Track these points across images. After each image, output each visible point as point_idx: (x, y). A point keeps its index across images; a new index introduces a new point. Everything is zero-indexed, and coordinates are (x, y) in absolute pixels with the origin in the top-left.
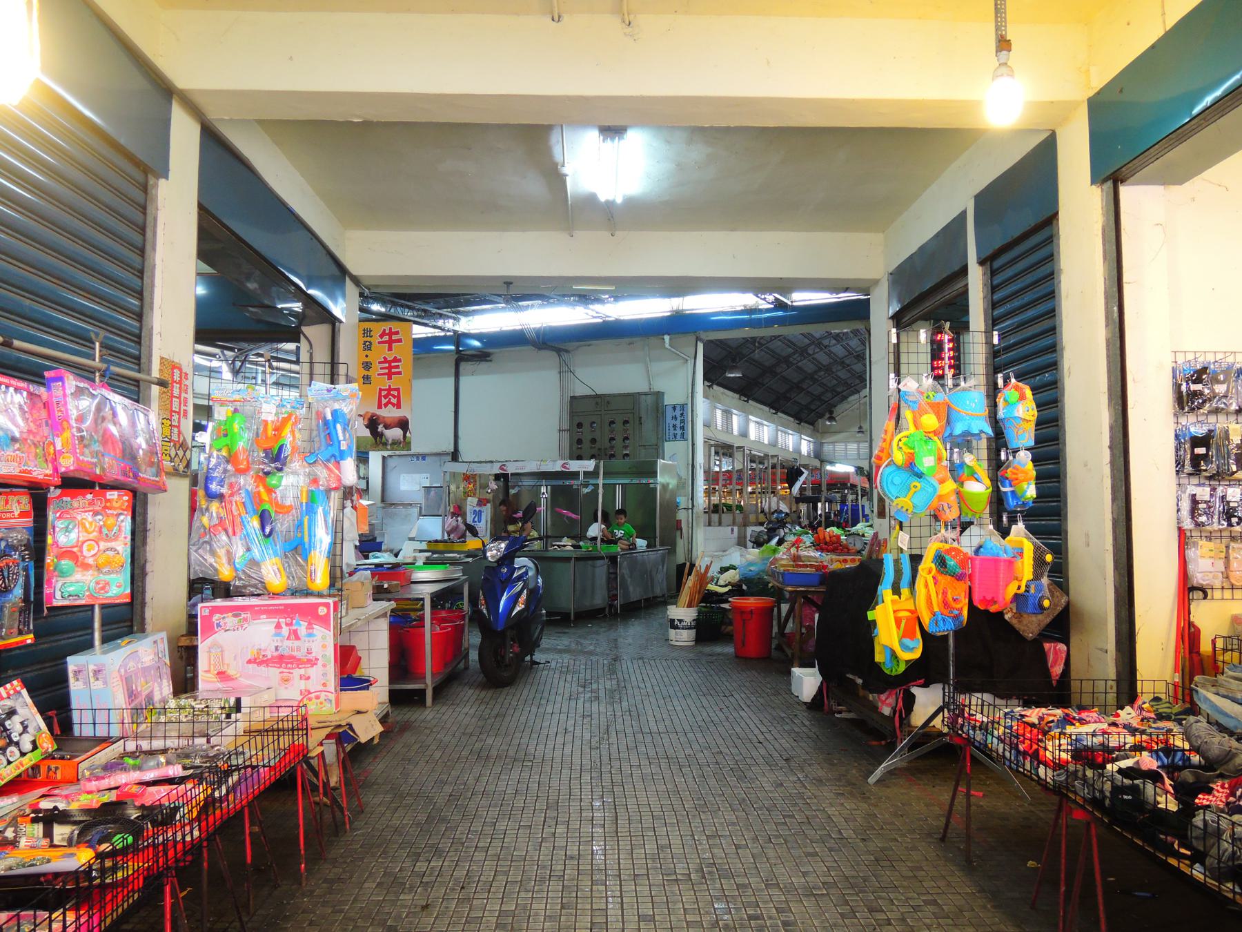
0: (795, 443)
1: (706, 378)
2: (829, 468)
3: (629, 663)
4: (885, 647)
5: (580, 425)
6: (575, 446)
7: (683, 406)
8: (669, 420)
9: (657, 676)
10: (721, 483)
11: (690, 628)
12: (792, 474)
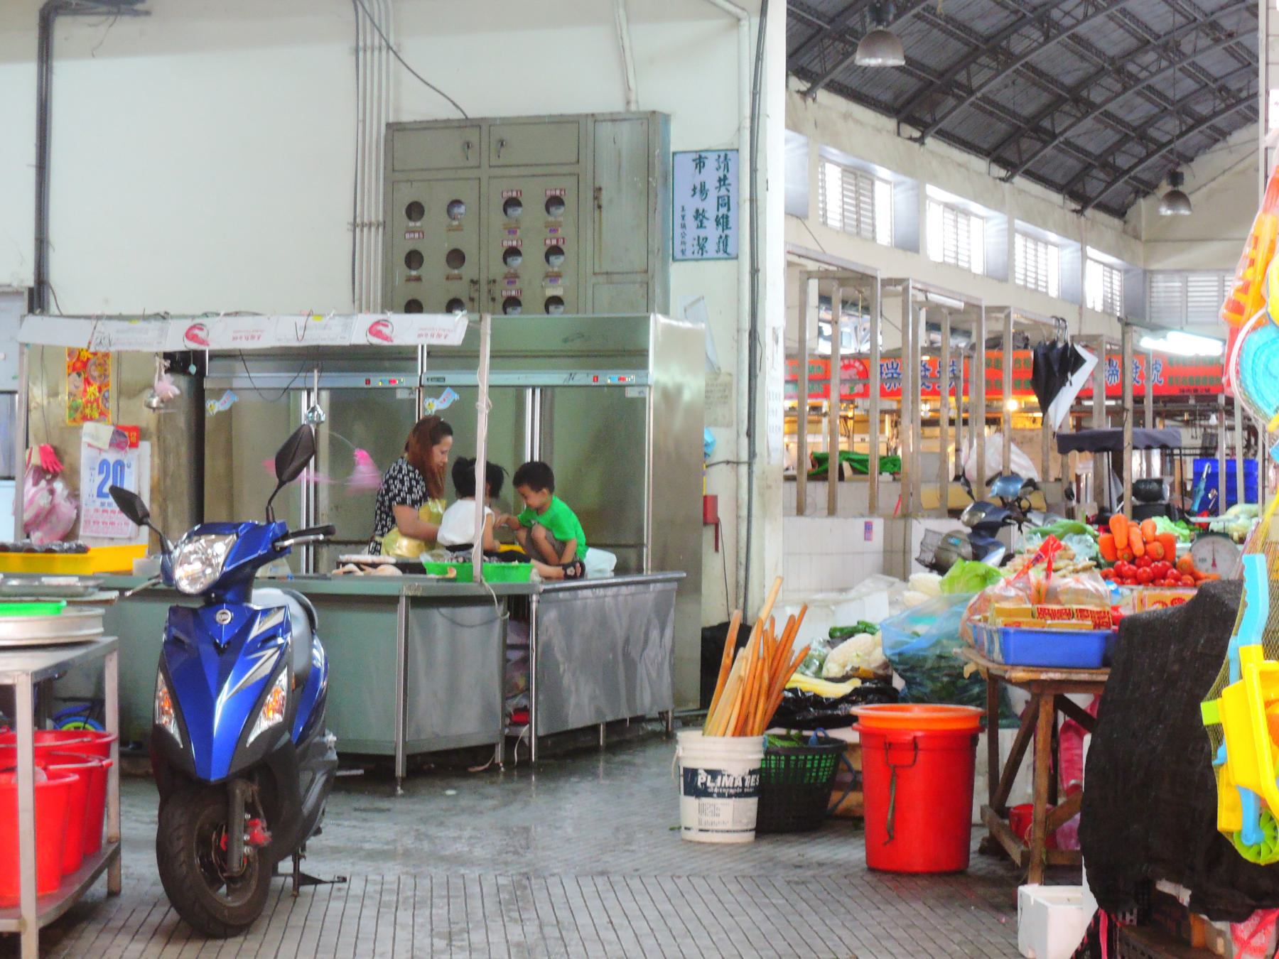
0: (1053, 265)
1: (796, 67)
2: (1148, 343)
3: (570, 885)
4: (1243, 790)
5: (415, 210)
6: (401, 270)
7: (726, 158)
8: (684, 199)
9: (651, 914)
10: (834, 395)
11: (742, 794)
12: (1050, 367)
